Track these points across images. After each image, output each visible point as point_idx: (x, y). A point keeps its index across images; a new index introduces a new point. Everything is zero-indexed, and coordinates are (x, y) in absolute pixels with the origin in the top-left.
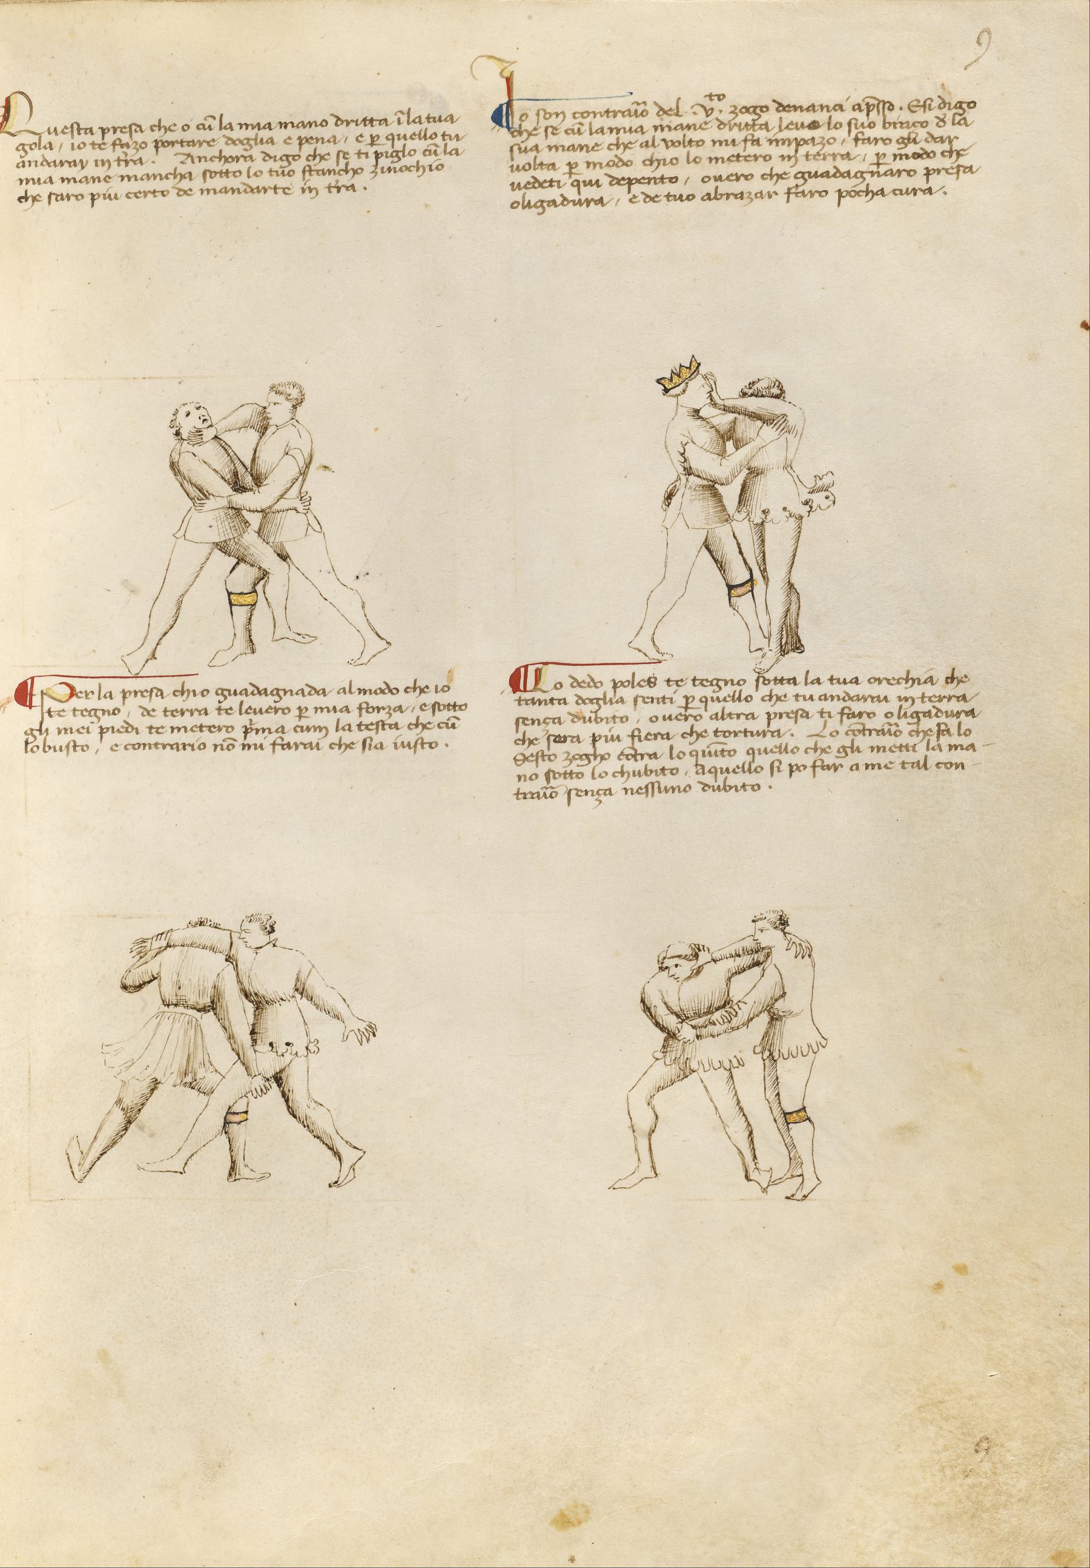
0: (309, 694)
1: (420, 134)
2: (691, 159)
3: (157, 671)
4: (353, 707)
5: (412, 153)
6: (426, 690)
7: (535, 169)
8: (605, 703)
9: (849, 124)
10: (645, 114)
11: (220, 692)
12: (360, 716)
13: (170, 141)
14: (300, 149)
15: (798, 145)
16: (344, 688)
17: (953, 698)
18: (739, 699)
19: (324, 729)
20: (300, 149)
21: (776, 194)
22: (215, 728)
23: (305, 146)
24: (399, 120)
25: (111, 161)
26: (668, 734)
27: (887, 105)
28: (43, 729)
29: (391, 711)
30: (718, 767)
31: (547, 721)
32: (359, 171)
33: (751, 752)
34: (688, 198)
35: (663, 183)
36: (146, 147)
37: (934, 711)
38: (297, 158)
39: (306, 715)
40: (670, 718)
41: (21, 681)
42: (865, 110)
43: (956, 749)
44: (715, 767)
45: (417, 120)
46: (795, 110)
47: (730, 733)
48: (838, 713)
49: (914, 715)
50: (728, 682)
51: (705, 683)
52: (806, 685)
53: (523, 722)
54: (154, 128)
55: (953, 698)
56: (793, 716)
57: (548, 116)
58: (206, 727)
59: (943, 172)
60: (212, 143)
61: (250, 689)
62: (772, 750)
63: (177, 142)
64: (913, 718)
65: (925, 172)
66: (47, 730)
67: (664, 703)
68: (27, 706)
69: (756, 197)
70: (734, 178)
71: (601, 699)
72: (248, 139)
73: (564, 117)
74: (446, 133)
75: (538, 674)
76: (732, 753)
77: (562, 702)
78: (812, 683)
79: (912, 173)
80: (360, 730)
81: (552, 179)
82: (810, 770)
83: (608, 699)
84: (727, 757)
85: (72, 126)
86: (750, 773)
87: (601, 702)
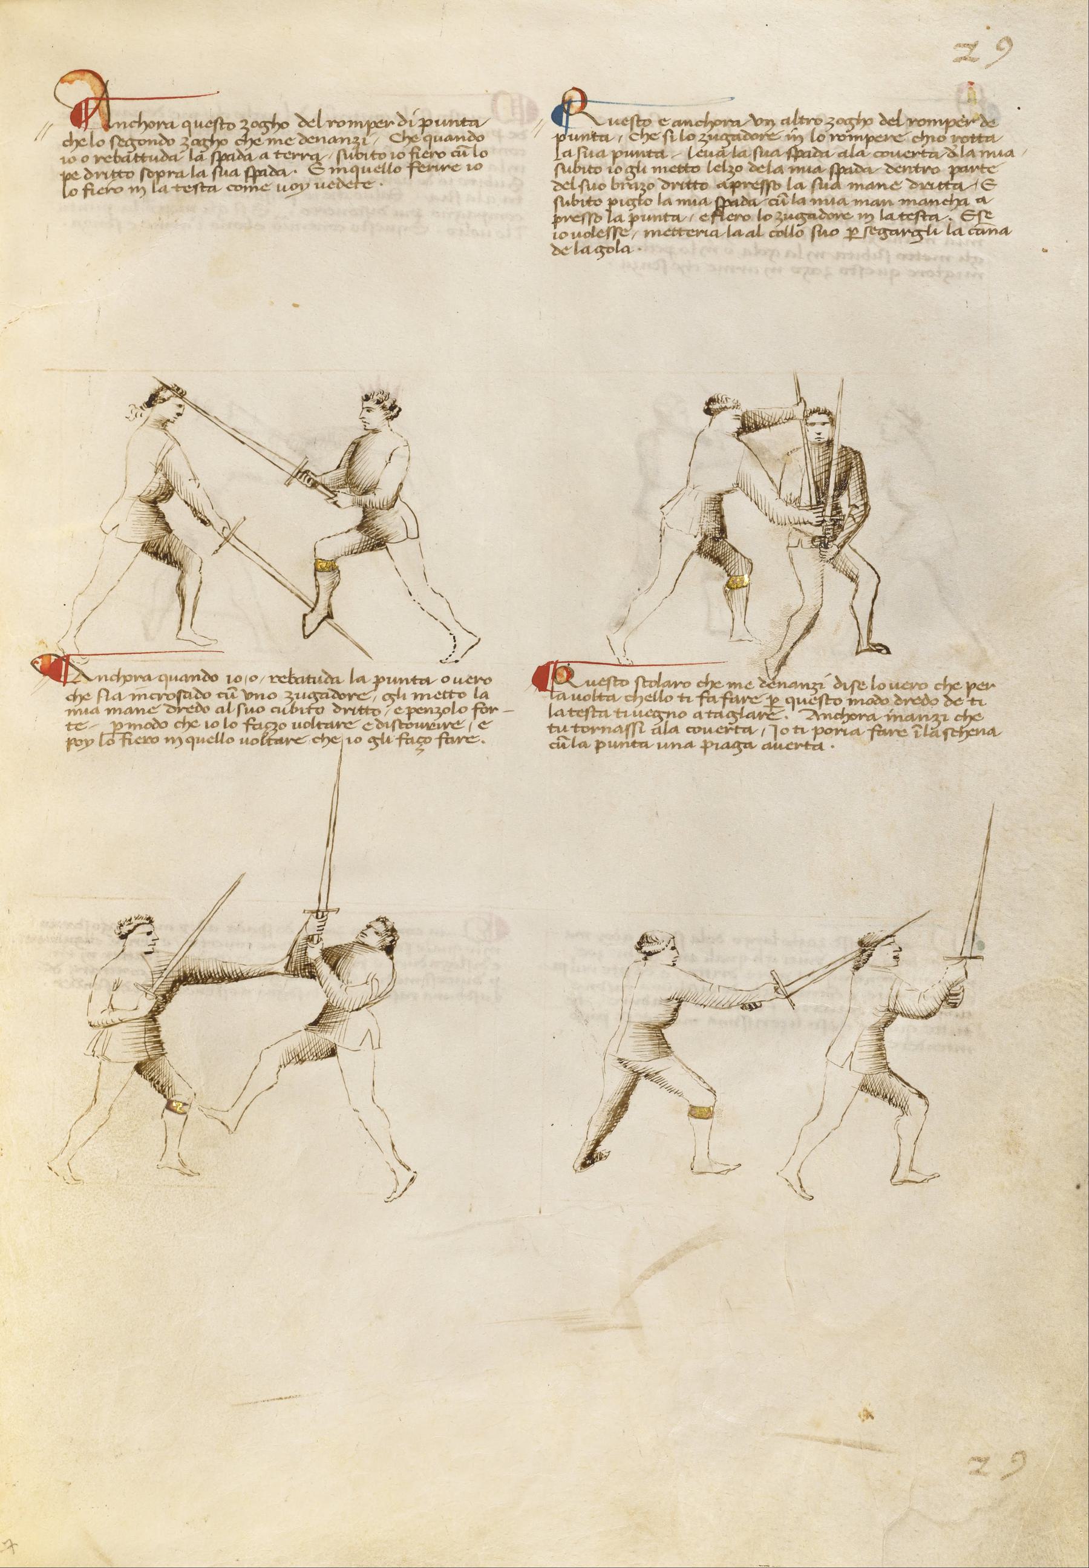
0: (271, 174)
1: (655, 695)
3: (292, 1564)
5: (463, 710)
6: (956, 686)
7: (594, 700)
11: (630, 203)
12: (701, 705)
13: (857, 714)
22: (110, 157)
24: (916, 732)
25: (603, 168)
26: (172, 123)
27: (594, 217)
28: (401, 694)
30: (795, 697)
32: (224, 142)
33: (837, 185)
34: (476, 169)
35: (600, 700)
36: (166, 726)
39: (857, 236)
41: (543, 663)
44: (792, 698)
46: (802, 688)
48: (572, 727)
50: (649, 233)
51: (691, 233)
53: (871, 231)
54: (316, 740)
58: (741, 728)
61: (202, 675)
62: (436, 695)
63: (801, 745)
66: (404, 695)
68: (60, 681)
70: (793, 746)
74: (684, 695)
76: (934, 171)
80: (571, 715)
81: (464, 119)
86: (247, 744)
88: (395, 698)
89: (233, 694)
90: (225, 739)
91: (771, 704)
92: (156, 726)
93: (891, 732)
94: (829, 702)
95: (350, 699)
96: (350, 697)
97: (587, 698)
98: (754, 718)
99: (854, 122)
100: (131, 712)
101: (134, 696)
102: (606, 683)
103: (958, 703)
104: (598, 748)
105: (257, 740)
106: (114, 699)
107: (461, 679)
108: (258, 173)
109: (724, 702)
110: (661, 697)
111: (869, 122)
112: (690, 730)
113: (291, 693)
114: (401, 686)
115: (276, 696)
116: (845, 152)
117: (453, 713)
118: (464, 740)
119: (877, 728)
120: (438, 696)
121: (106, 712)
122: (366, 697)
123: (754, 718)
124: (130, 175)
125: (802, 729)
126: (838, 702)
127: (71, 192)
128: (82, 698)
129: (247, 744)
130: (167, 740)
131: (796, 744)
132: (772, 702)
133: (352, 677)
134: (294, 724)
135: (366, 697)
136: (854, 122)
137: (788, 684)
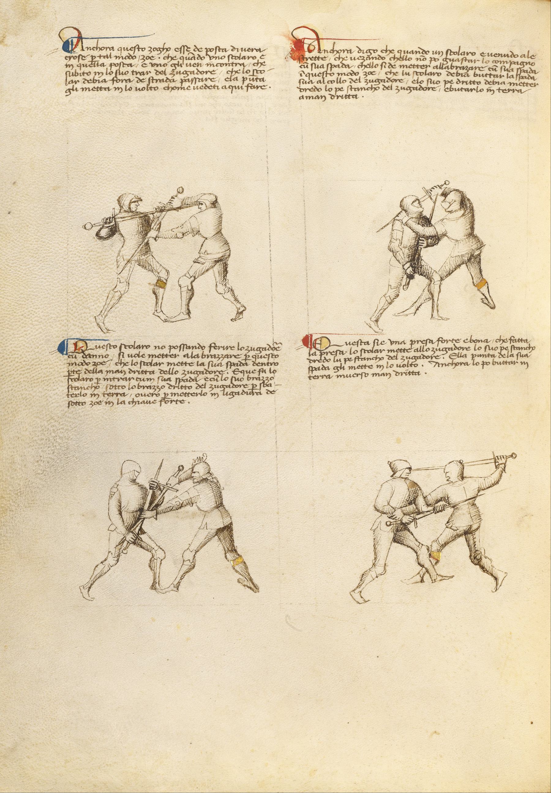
2: (272, 371)
4: (184, 66)
8: (178, 66)
9: (382, 65)
10: (533, 64)
14: (430, 63)
15: (511, 64)
16: (524, 55)
17: (470, 54)
18: (96, 372)
19: (323, 97)
20: (430, 63)
21: (163, 364)
23: (433, 62)
29: (367, 74)
31: (218, 65)
37: (341, 65)
38: (190, 388)
40: (99, 347)
42: (461, 61)
43: (505, 55)
45: (322, 66)
47: (223, 64)
49: (522, 64)
51: (73, 396)
52: (118, 404)
54: (165, 58)
55: (470, 54)
56: (133, 49)
57: (73, 404)
59: (398, 81)
60: (191, 364)
64: (521, 65)
65: (411, 343)
67: (151, 90)
69: (369, 74)
71: (176, 64)
72: (160, 48)
73: (113, 404)
75: (67, 341)
77: (366, 343)
78: (312, 355)
79: (474, 54)
82: (380, 67)
83: (180, 64)
84: (87, 83)
85: (107, 345)
86: (245, 51)
87: (176, 66)
88: (71, 91)
89: (307, 65)
90: (174, 372)
91: (69, 374)
92: (130, 57)
93: (257, 87)
94: (111, 347)
95: (463, 84)
96: (157, 66)
97: (143, 89)
98: (413, 54)
99: (162, 50)
100: (157, 365)
101: (389, 351)
102: (335, 353)
103: (273, 392)
104: (483, 365)
105: (144, 88)
106: (313, 355)
107: (355, 58)
108: (209, 50)
109: (259, 373)
110: (340, 81)
111: (169, 49)
112: (329, 82)
113: (185, 371)
114: (373, 61)
115: (178, 372)
116: (437, 66)
117: (458, 55)
118: (478, 68)
119: (213, 345)
120: (202, 88)
121: (167, 364)
122: (239, 357)
123: (413, 54)
124: (143, 50)
125: (218, 86)
126: (190, 388)
127: (481, 90)
128: (380, 359)
129: (245, 51)
130: (83, 89)
131: (262, 363)
132: (253, 387)
133: (351, 352)
134: (397, 365)
135: (239, 357)
136: (162, 50)
137: (162, 65)
